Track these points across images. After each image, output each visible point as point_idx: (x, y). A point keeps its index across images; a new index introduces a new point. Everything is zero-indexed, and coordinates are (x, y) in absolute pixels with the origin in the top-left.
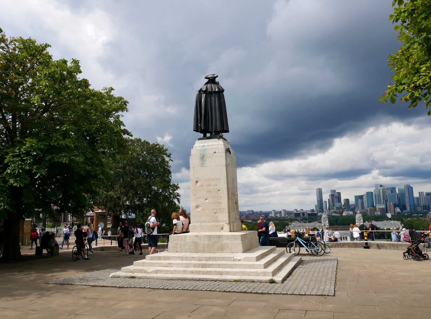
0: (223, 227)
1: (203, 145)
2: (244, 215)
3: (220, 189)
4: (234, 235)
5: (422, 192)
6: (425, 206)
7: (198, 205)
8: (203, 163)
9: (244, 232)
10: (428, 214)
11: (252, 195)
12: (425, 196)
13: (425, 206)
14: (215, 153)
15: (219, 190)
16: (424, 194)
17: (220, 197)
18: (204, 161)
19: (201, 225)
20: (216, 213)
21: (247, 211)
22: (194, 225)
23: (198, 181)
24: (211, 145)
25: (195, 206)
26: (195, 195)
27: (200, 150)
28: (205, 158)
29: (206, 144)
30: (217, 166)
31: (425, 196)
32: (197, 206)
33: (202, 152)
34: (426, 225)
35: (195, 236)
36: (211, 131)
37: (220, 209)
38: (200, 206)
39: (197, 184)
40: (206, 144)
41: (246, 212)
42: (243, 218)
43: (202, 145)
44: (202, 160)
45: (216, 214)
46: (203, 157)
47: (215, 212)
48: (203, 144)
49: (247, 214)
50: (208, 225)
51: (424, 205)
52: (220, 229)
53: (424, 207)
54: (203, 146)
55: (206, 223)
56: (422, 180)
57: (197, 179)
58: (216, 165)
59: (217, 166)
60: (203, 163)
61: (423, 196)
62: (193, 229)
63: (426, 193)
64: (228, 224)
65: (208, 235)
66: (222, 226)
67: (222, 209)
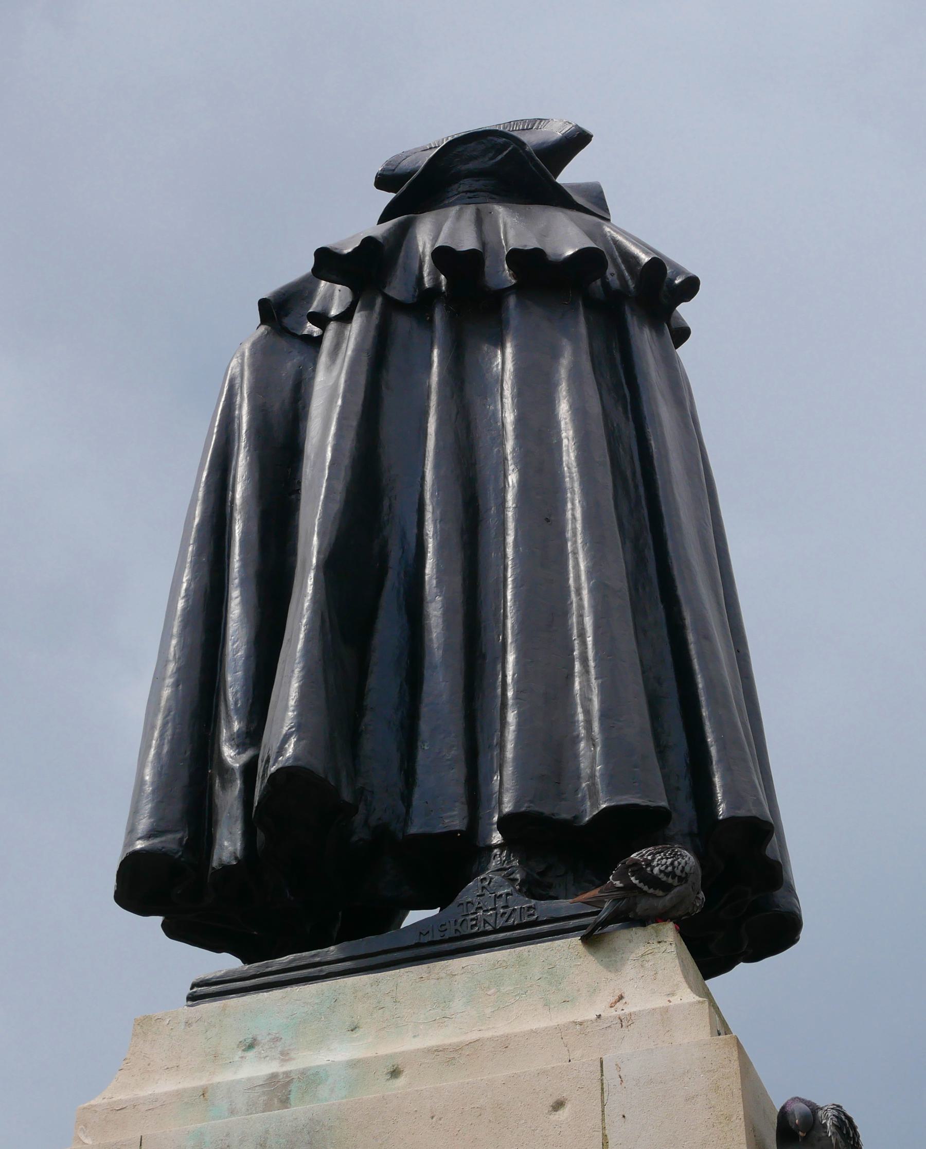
1: (272, 1067)
48: (285, 1056)
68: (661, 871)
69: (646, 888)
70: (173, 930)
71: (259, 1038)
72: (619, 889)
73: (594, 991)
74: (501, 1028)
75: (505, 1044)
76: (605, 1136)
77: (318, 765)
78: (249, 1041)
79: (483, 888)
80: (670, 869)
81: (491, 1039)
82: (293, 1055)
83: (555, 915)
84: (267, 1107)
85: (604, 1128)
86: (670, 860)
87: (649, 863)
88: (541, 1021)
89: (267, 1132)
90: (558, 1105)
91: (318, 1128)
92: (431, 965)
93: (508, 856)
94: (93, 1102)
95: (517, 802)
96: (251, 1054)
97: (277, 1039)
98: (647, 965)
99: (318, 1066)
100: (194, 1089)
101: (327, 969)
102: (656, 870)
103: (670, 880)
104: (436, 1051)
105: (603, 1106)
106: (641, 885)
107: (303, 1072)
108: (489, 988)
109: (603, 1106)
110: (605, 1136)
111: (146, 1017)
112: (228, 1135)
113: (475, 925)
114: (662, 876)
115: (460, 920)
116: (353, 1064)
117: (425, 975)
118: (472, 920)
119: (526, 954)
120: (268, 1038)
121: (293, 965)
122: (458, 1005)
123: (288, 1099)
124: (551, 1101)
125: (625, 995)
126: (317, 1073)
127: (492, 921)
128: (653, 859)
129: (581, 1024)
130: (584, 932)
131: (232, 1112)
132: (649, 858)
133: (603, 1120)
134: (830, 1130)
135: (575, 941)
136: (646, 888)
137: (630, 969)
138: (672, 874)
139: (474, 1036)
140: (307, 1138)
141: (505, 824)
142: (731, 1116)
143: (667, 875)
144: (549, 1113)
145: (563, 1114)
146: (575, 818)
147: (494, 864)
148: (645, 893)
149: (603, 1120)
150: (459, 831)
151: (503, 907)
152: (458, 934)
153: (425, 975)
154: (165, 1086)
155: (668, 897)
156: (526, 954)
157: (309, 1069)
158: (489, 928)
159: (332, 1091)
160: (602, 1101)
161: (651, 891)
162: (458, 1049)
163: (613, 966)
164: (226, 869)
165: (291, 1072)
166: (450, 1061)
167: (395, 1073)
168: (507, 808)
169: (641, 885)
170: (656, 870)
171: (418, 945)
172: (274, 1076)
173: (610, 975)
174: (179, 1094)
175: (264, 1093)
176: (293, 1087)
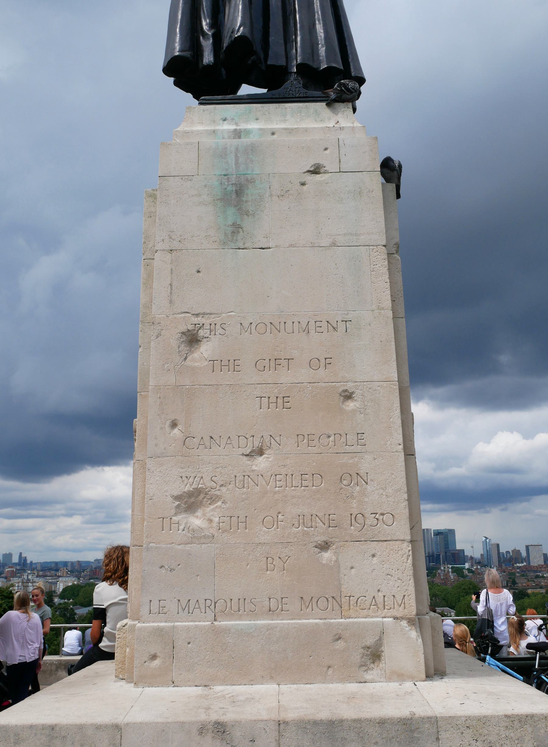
0: (379, 643)
1: (233, 127)
2: (88, 570)
3: (350, 386)
4: (532, 716)
5: (427, 530)
6: (433, 556)
7: (198, 492)
8: (236, 228)
9: (508, 670)
10: (439, 571)
11: (112, 527)
12: (433, 536)
13: (433, 556)
14: (316, 170)
15: (348, 396)
16: (431, 533)
17: (352, 438)
18: (243, 212)
19: (218, 632)
20: (325, 546)
21: (95, 560)
22: (159, 630)
23: (201, 333)
24: (289, 131)
25: (177, 498)
26: (174, 425)
27: (222, 154)
28: (251, 193)
29: (253, 126)
30: (334, 244)
31: (433, 536)
32: (190, 494)
33: (231, 159)
34: (438, 591)
35: (202, 730)
36: (284, 64)
37: (353, 518)
38: (213, 499)
39: (196, 355)
40: (253, 126)
41: (92, 562)
42: (85, 575)
43: (228, 127)
44: (231, 211)
45: (327, 556)
46: (239, 192)
47: (321, 539)
48: (236, 124)
49: (94, 566)
50: (269, 628)
51: (431, 554)
52: (356, 657)
53: (431, 558)
54: (238, 134)
55: (253, 614)
56: (436, 506)
57: (196, 320)
58: (325, 242)
59: (334, 244)
60: (236, 228)
61: (430, 535)
62: (154, 657)
63: (434, 530)
64: (411, 621)
65: (316, 723)
66: (370, 641)
67: (371, 520)
68: (351, 87)
69: (346, 91)
70: (176, 84)
71: (227, 118)
72: (339, 90)
73: (329, 119)
74: (303, 125)
75: (306, 130)
76: (340, 159)
77: (248, 35)
78: (224, 118)
79: (292, 84)
80: (353, 87)
81: (302, 128)
82: (239, 124)
83: (314, 96)
84: (234, 138)
85: (339, 157)
86: (353, 85)
87: (348, 84)
88: (316, 125)
89: (238, 145)
90: (326, 149)
91: (254, 146)
92: (280, 104)
93: (297, 76)
94: (177, 129)
95: (303, 59)
96: (225, 122)
97: (233, 119)
98: (345, 114)
99: (250, 128)
100: (211, 130)
101: (243, 101)
102: (350, 87)
103: (353, 91)
104: (286, 129)
105: (339, 151)
106: (345, 90)
107: (245, 130)
108: (298, 114)
109: (339, 151)
110: (340, 159)
111: (190, 107)
112: (226, 144)
113: (289, 95)
114: (351, 89)
115: (285, 92)
116: (260, 129)
117: (278, 107)
118: (289, 93)
119: (308, 105)
120: (230, 119)
121: (233, 98)
122: (288, 117)
123: (240, 137)
124: (324, 148)
125: (339, 121)
126: (249, 130)
127: (294, 94)
128: (349, 84)
129: (329, 127)
130: (327, 102)
131: (223, 138)
132: (348, 83)
133: (339, 155)
134: (397, 166)
135: (324, 104)
136: (346, 91)
137: (340, 115)
138: (354, 89)
139: (297, 127)
140: (251, 148)
141: (298, 66)
142: (376, 159)
143: (352, 89)
144: (324, 151)
145: (327, 152)
146: (318, 68)
147: (292, 79)
148: (346, 93)
149: (339, 155)
150: (284, 66)
151: (298, 91)
152: (284, 97)
153: (278, 107)
154: (200, 128)
155: (351, 95)
156: (308, 105)
157: (247, 129)
158: (294, 96)
159: (254, 136)
160: (339, 150)
161: (347, 92)
162: (292, 129)
163: (336, 113)
164: (208, 66)
165: (241, 129)
166: (290, 133)
167: (273, 134)
168: (299, 61)
169: (345, 90)
170: (350, 87)
171: (298, 97)
172: (236, 129)
173: (334, 115)
174: (206, 131)
175: (233, 134)
176: (242, 134)
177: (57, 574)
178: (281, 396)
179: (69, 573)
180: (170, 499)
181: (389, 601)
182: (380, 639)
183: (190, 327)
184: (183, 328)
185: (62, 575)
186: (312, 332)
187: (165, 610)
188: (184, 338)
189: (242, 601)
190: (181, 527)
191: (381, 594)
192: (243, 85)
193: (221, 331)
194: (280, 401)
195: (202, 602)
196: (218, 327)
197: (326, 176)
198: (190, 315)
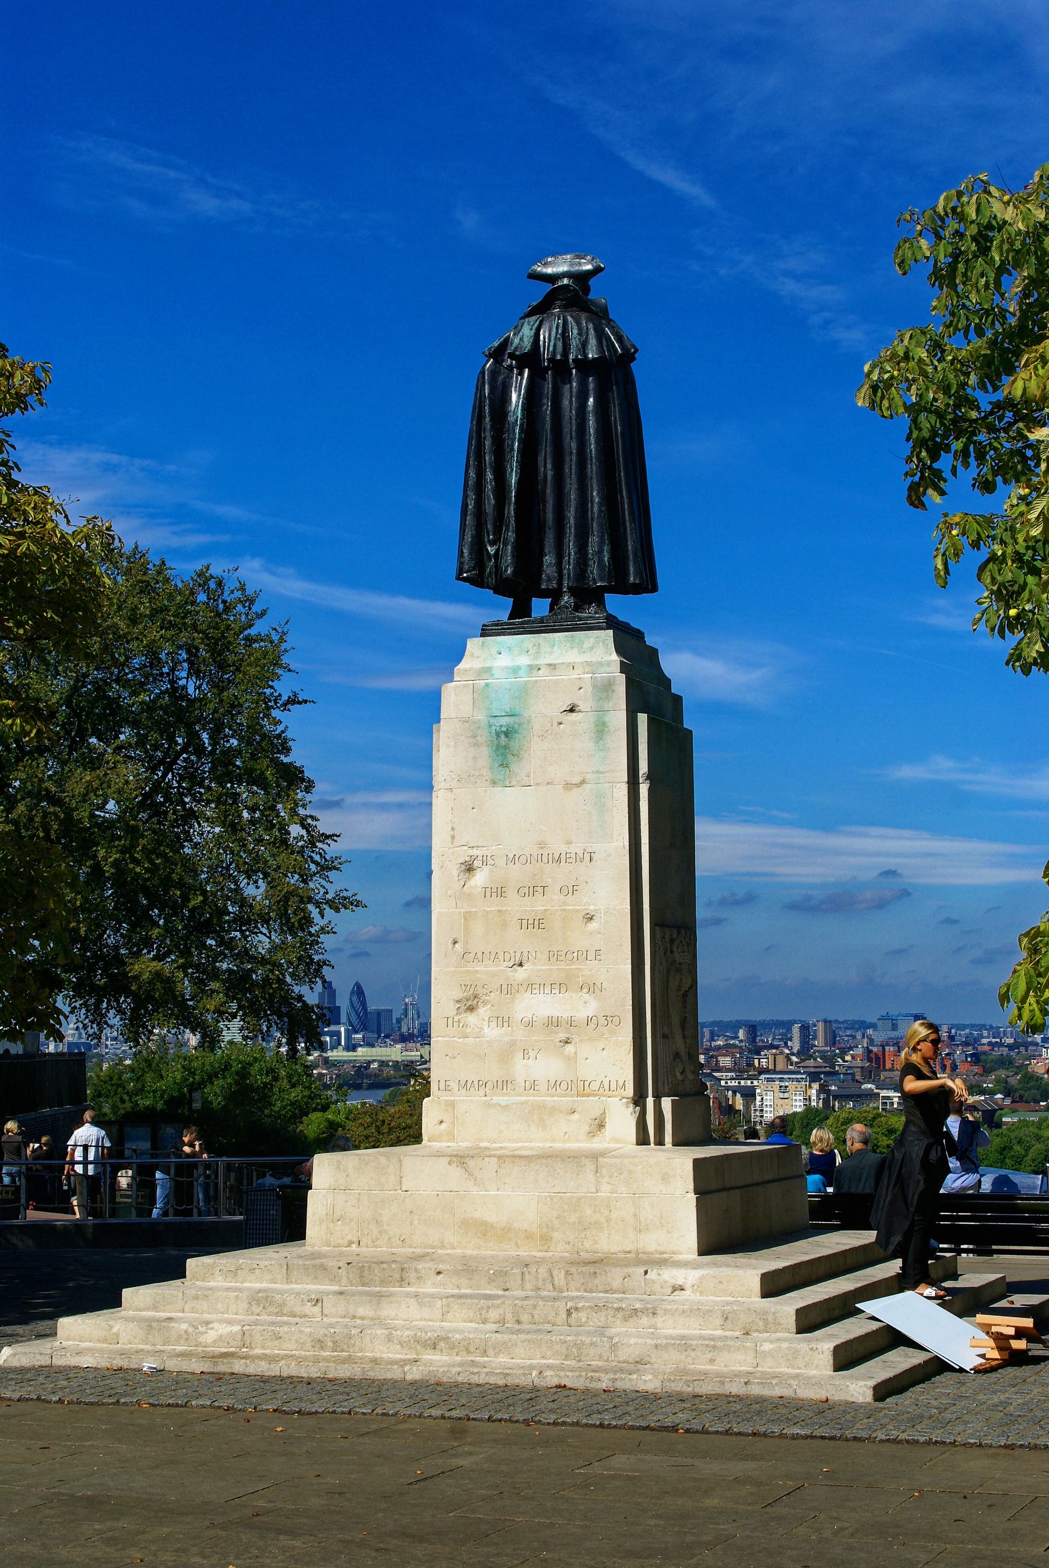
46: (508, 733)
90: (580, 688)
177: (756, 1062)
178: (538, 918)
179: (794, 1059)
180: (452, 1003)
181: (613, 1086)
182: (604, 1113)
183: (467, 859)
184: (462, 860)
185: (771, 1067)
186: (563, 862)
187: (450, 1088)
188: (463, 867)
189: (505, 1082)
190: (461, 1025)
191: (608, 1079)
192: (188, 1260)
193: (492, 862)
194: (536, 922)
195: (476, 1083)
196: (489, 858)
197: (581, 715)
198: (466, 848)
